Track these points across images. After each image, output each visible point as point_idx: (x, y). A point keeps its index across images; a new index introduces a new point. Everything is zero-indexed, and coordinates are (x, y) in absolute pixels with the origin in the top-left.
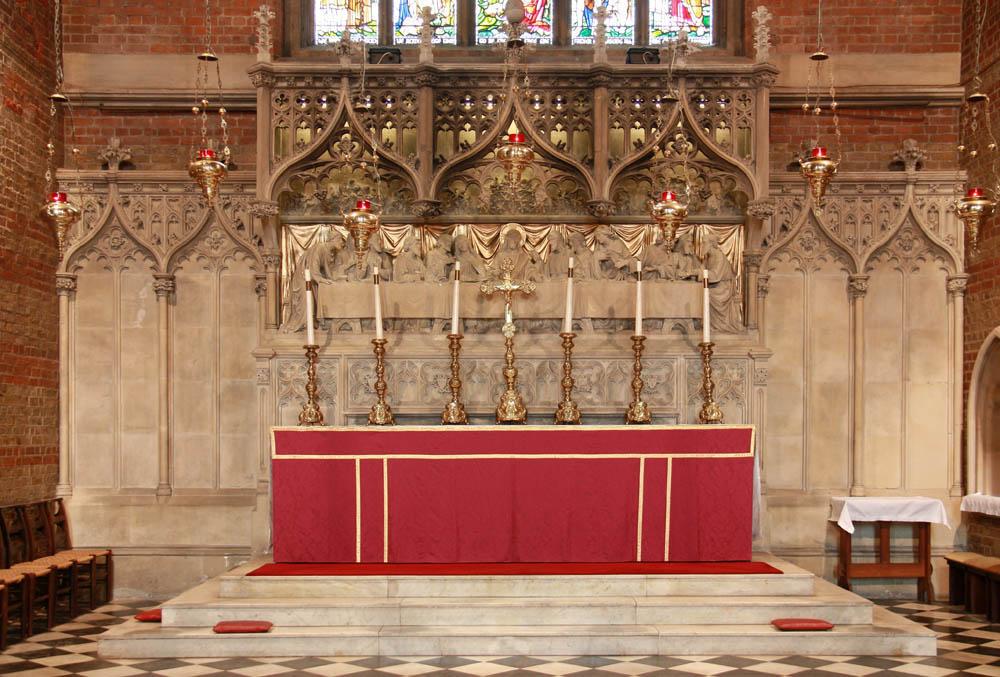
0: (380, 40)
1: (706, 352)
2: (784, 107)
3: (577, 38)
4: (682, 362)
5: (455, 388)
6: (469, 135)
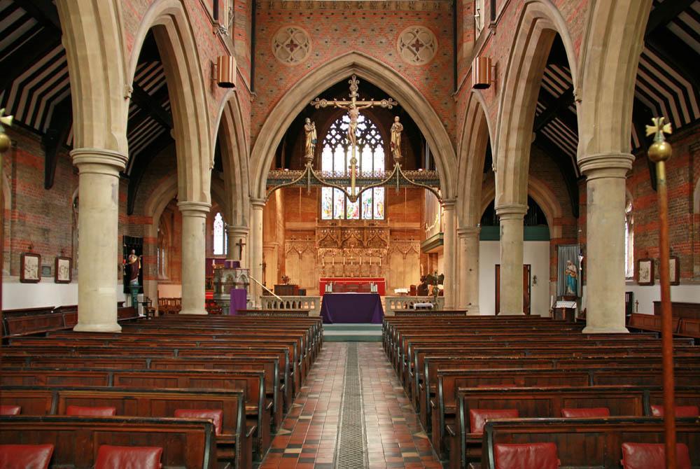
0: (320, 191)
1: (380, 267)
2: (392, 231)
3: (363, 218)
4: (377, 269)
5: (344, 272)
6: (346, 236)
